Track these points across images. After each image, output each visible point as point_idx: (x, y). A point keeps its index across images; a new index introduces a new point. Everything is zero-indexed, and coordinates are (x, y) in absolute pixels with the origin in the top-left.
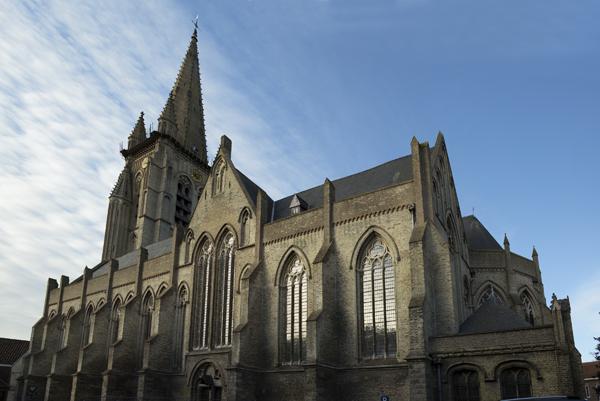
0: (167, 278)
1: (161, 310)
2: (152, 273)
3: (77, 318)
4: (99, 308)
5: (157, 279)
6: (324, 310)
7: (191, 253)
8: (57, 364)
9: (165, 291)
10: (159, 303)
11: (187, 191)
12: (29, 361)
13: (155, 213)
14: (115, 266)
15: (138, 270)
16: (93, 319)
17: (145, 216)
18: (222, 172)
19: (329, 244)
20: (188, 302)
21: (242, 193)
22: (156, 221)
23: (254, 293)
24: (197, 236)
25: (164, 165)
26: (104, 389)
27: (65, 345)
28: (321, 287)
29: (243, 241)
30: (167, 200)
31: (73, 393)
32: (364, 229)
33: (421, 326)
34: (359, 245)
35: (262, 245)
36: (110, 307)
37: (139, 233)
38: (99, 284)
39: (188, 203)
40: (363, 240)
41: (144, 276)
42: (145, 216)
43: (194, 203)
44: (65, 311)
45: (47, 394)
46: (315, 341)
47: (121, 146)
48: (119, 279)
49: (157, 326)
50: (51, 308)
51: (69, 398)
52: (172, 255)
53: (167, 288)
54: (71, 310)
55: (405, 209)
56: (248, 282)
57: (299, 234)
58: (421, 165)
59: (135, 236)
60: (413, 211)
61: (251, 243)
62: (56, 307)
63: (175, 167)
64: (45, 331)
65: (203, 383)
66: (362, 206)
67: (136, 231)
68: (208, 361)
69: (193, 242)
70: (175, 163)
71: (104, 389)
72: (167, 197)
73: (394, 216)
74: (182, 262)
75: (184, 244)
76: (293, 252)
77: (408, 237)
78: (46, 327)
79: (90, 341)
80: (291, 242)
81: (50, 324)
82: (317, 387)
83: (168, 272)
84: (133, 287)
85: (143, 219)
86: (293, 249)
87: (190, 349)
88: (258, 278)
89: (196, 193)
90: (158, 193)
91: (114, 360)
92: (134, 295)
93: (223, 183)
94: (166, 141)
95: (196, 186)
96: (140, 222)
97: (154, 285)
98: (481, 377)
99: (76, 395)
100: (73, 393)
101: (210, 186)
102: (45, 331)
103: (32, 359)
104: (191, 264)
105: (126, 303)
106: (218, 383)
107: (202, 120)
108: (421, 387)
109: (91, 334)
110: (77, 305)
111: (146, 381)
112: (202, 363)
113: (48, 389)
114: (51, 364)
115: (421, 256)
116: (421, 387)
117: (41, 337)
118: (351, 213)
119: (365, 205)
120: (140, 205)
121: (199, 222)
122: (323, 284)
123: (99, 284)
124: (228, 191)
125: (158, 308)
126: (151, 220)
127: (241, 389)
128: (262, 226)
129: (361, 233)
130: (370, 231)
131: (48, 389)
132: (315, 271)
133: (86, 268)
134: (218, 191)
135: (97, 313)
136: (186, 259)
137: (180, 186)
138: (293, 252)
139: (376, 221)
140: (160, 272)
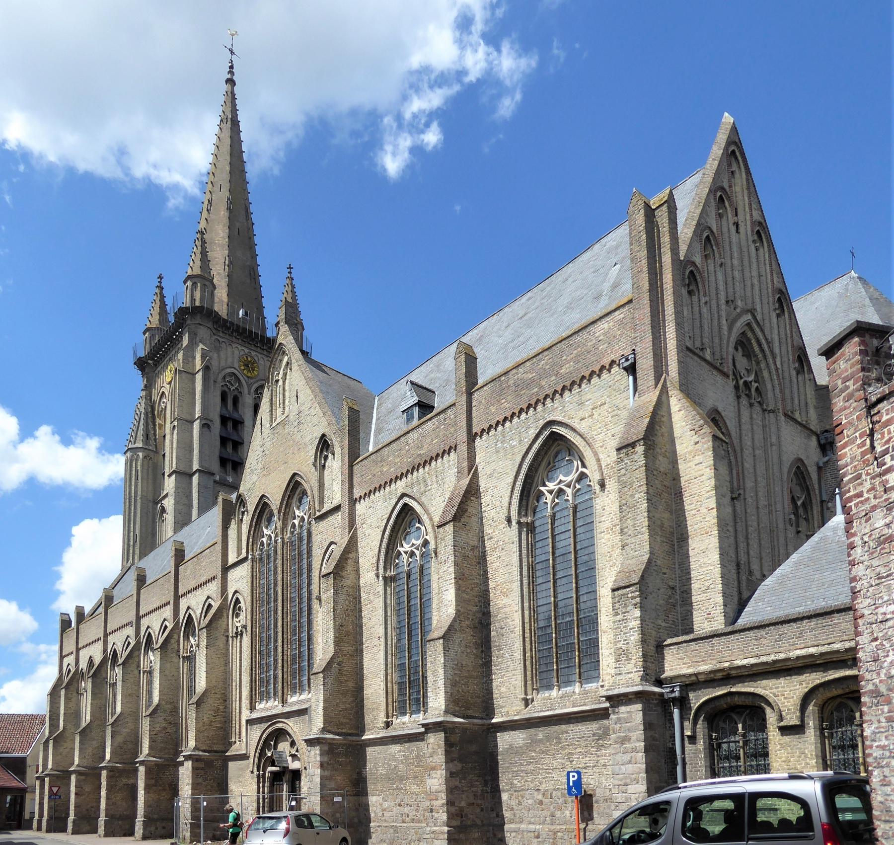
0: (213, 589)
2: (193, 584)
3: (98, 673)
5: (199, 592)
6: (458, 612)
8: (81, 749)
9: (212, 611)
10: (204, 634)
11: (236, 401)
13: (191, 466)
14: (141, 580)
15: (172, 580)
17: (179, 420)
18: (285, 375)
19: (466, 481)
20: (245, 627)
21: (317, 410)
22: (191, 475)
23: (342, 597)
24: (251, 507)
26: (141, 784)
28: (452, 569)
29: (322, 502)
30: (206, 429)
31: (103, 793)
32: (533, 432)
33: (636, 623)
35: (353, 502)
36: (139, 650)
37: (169, 503)
38: (122, 614)
39: (238, 424)
40: (531, 455)
41: (181, 591)
42: (174, 472)
43: (248, 422)
44: (83, 665)
46: (442, 676)
47: (135, 353)
48: (150, 600)
49: (204, 675)
50: (66, 661)
52: (219, 547)
53: (216, 605)
54: (91, 661)
55: (615, 369)
56: (331, 581)
57: (414, 468)
58: (526, 452)
59: (163, 510)
60: (632, 369)
61: (335, 503)
63: (215, 364)
65: (273, 765)
66: (528, 384)
67: (165, 502)
69: (247, 519)
70: (215, 355)
71: (141, 784)
73: (592, 391)
74: (232, 559)
75: (233, 526)
76: (406, 505)
77: (614, 443)
78: (63, 692)
79: (119, 709)
80: (400, 486)
82: (446, 762)
83: (214, 578)
84: (168, 612)
86: (406, 500)
87: (252, 709)
88: (350, 568)
90: (192, 422)
91: (150, 738)
92: (170, 626)
93: (287, 394)
94: (198, 320)
95: (249, 386)
96: (170, 484)
97: (194, 603)
98: (771, 718)
99: (108, 798)
100: (103, 793)
101: (268, 404)
103: (51, 742)
104: (246, 559)
105: (161, 641)
106: (294, 765)
107: (254, 256)
108: (635, 750)
109: (119, 697)
110: (96, 653)
112: (270, 729)
113: (73, 789)
115: (641, 474)
116: (635, 750)
119: (532, 380)
120: (167, 455)
121: (255, 478)
122: (456, 564)
123: (122, 614)
125: (204, 643)
126: (184, 475)
127: (327, 773)
128: (351, 467)
129: (527, 442)
130: (546, 433)
131: (73, 789)
132: (443, 539)
134: (279, 411)
135: (124, 663)
136: (239, 552)
137: (224, 397)
139: (555, 411)
140: (204, 579)
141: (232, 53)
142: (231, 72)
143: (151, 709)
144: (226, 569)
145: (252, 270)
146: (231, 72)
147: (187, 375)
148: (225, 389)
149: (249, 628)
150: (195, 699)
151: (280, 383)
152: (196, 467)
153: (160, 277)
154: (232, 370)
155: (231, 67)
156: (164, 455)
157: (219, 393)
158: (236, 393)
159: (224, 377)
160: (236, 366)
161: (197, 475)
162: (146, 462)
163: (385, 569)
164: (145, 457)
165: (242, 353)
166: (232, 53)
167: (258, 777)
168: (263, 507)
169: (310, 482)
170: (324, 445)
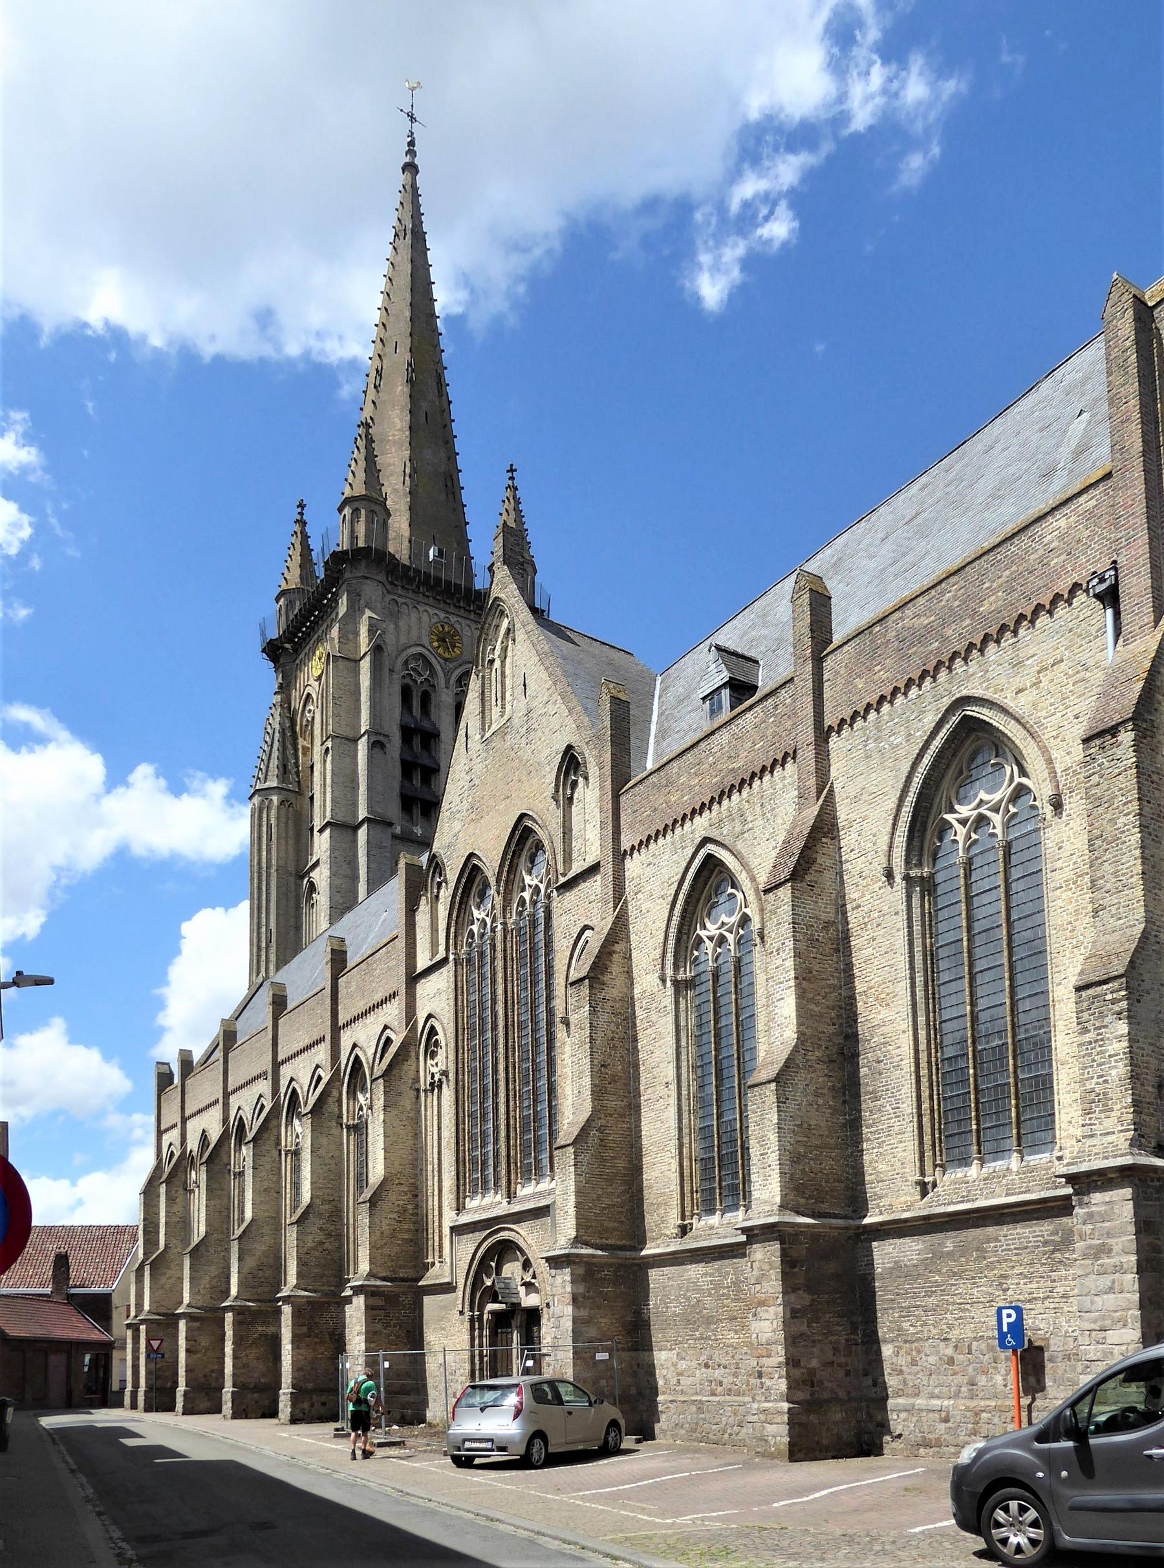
0: (393, 1012)
1: (386, 1108)
2: (361, 1007)
4: (257, 1125)
5: (370, 1018)
7: (442, 926)
9: (393, 1050)
11: (426, 699)
12: (143, 1276)
14: (279, 1004)
15: (328, 1001)
16: (247, 1151)
20: (445, 1073)
25: (364, 648)
27: (203, 1229)
28: (790, 963)
30: (377, 750)
31: (229, 1348)
32: (930, 720)
34: (917, 781)
35: (620, 857)
43: (445, 735)
45: (182, 1355)
51: (1155, 1169)
53: (397, 1039)
55: (1081, 598)
56: (585, 990)
57: (724, 794)
59: (312, 888)
60: (1111, 597)
61: (590, 860)
62: (173, 1136)
64: (163, 1199)
68: (504, 1235)
69: (446, 894)
72: (377, 745)
74: (423, 962)
75: (424, 906)
76: (709, 857)
80: (700, 826)
81: (168, 1182)
84: (322, 1054)
85: (327, 832)
86: (710, 848)
87: (460, 1208)
88: (616, 968)
89: (445, 697)
95: (447, 675)
96: (322, 844)
101: (478, 701)
102: (163, 1199)
103: (147, 1269)
104: (445, 961)
106: (530, 1300)
108: (1119, 1269)
110: (212, 1124)
111: (368, 1308)
114: (181, 1279)
117: (845, 1489)
118: (885, 676)
119: (929, 628)
121: (457, 825)
122: (797, 954)
124: (521, 705)
125: (379, 1103)
127: (584, 1313)
129: (920, 737)
133: (184, 938)
135: (254, 1140)
138: (709, 857)
140: (378, 997)
141: (412, 118)
142: (411, 152)
143: (299, 1212)
144: (413, 979)
145: (449, 479)
146: (411, 152)
147: (346, 662)
148: (408, 681)
149: (452, 1076)
150: (367, 1194)
151: (497, 664)
152: (362, 813)
153: (301, 506)
154: (420, 649)
155: (411, 143)
156: (312, 798)
157: (397, 689)
158: (426, 687)
159: (406, 663)
160: (426, 642)
161: (365, 826)
162: (283, 811)
163: (676, 967)
164: (282, 803)
165: (435, 620)
166: (412, 118)
167: (472, 1320)
168: (471, 872)
169: (548, 829)
170: (571, 763)
